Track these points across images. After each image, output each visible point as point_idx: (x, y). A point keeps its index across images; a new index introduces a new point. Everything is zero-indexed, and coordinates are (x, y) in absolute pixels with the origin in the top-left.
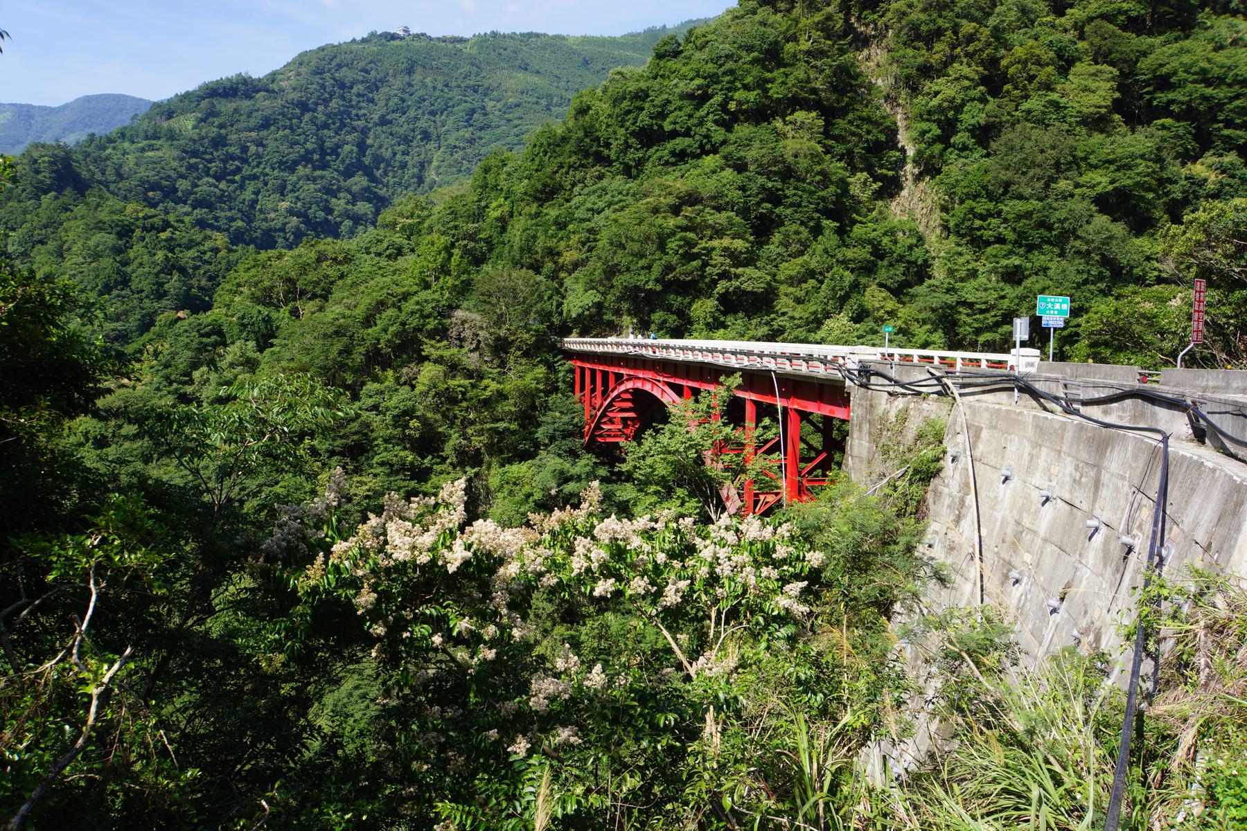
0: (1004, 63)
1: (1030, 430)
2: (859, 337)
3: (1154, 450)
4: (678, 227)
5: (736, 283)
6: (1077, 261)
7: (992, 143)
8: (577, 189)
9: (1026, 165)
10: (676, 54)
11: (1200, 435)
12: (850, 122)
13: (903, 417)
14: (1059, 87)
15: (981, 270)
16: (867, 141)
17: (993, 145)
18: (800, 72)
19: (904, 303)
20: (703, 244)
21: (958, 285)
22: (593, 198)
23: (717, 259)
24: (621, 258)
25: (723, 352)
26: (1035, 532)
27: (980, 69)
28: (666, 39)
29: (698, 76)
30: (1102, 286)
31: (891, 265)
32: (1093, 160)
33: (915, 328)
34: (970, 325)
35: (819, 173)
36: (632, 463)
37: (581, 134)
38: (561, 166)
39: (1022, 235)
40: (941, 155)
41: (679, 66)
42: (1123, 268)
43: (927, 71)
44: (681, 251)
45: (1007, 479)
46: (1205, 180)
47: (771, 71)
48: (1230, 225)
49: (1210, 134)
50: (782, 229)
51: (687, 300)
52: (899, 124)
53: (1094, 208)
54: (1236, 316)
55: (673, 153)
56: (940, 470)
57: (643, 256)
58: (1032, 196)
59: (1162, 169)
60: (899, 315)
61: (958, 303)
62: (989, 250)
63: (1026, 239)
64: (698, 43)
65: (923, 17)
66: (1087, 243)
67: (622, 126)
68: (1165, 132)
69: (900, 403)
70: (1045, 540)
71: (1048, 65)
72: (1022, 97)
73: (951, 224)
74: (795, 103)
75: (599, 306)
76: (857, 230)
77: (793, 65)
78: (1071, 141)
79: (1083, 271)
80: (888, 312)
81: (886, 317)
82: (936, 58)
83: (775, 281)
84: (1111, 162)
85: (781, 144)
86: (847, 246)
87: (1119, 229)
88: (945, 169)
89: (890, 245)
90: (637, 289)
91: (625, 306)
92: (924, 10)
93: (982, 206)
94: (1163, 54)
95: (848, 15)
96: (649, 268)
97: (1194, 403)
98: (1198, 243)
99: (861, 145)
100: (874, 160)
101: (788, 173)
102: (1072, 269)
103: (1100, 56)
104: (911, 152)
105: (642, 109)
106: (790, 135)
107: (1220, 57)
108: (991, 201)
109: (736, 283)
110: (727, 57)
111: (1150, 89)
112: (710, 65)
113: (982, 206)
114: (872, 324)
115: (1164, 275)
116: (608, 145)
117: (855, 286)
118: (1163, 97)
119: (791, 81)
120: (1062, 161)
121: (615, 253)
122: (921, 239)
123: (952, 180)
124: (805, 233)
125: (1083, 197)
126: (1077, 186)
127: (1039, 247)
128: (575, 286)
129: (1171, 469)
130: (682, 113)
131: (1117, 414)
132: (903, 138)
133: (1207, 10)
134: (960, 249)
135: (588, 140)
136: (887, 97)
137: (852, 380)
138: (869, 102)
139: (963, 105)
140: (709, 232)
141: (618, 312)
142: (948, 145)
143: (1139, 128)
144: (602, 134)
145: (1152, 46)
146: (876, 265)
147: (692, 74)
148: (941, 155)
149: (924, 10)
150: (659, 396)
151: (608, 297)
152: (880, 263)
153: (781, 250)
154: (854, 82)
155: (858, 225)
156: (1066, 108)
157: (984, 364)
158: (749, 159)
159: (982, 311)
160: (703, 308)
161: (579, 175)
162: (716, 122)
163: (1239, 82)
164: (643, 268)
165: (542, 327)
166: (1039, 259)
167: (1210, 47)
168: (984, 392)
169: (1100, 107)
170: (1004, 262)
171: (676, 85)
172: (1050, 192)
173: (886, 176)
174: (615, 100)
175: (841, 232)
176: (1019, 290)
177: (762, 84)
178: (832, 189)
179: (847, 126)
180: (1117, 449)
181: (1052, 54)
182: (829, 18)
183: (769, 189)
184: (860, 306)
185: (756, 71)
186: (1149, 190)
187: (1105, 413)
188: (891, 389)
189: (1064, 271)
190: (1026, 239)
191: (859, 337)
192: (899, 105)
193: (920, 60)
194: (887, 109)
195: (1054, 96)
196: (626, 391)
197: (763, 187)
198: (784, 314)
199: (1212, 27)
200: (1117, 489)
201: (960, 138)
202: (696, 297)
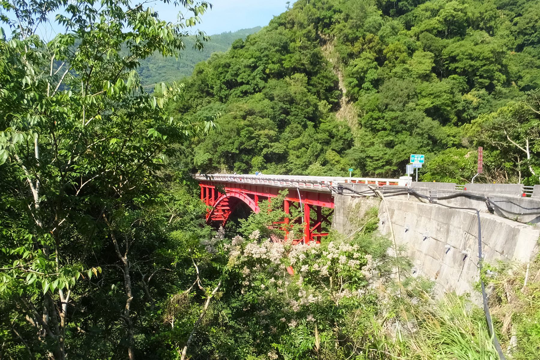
0: (385, 51)
1: (416, 210)
2: (325, 172)
3: (474, 217)
4: (245, 125)
5: (271, 150)
6: (418, 138)
7: (380, 87)
8: (198, 108)
9: (395, 96)
10: (242, 47)
11: (491, 211)
12: (319, 78)
13: (358, 206)
14: (408, 62)
15: (376, 142)
16: (326, 86)
17: (381, 88)
18: (297, 56)
19: (343, 157)
20: (256, 132)
21: (366, 149)
22: (206, 112)
23: (263, 139)
24: (220, 139)
25: (274, 180)
26: (421, 252)
27: (375, 54)
28: (237, 40)
29: (252, 57)
30: (429, 148)
31: (337, 141)
32: (424, 94)
33: (348, 168)
34: (372, 166)
35: (305, 101)
36: (244, 228)
37: (200, 82)
38: (191, 97)
39: (394, 127)
40: (358, 92)
41: (244, 52)
42: (438, 140)
43: (351, 55)
44: (247, 136)
45: (407, 230)
46: (472, 101)
47: (284, 55)
48: (491, 124)
49: (473, 81)
50: (290, 126)
51: (250, 157)
52: (340, 79)
53: (425, 114)
54: (495, 162)
55: (242, 92)
56: (377, 228)
57: (230, 138)
58: (397, 110)
59: (454, 97)
60: (341, 162)
61: (366, 157)
62: (379, 133)
63: (395, 128)
64: (252, 42)
65: (350, 31)
66: (422, 130)
67: (219, 79)
68: (454, 81)
69: (357, 200)
70: (426, 255)
71: (403, 52)
72: (393, 67)
73: (363, 123)
74: (295, 70)
75: (210, 160)
76: (322, 126)
77: (294, 53)
78: (414, 85)
79: (420, 142)
80: (337, 162)
81: (335, 163)
82: (355, 50)
83: (287, 148)
84: (432, 94)
85: (289, 88)
86: (318, 133)
87: (436, 123)
88: (359, 98)
89: (336, 132)
90: (228, 152)
91: (222, 160)
92: (350, 28)
93: (376, 114)
94: (453, 47)
95: (317, 30)
96: (233, 143)
97: (488, 198)
98: (478, 131)
99: (323, 88)
100: (329, 95)
101: (292, 101)
102: (415, 141)
103: (427, 48)
104: (345, 91)
105: (227, 72)
106: (292, 84)
107: (477, 48)
108: (380, 112)
109: (271, 150)
110: (265, 49)
111: (448, 62)
112: (258, 52)
113: (376, 114)
114: (330, 167)
115: (456, 143)
116: (212, 88)
117: (322, 150)
118: (453, 66)
119: (293, 60)
120: (410, 94)
121: (218, 136)
122: (349, 129)
123: (363, 104)
124: (300, 128)
125: (420, 110)
126: (417, 105)
127: (401, 132)
128: (199, 151)
129: (481, 224)
130: (245, 74)
131: (453, 203)
132: (341, 85)
133: (470, 27)
134: (367, 133)
135: (203, 85)
136: (334, 67)
137: (335, 191)
138: (326, 69)
139: (367, 70)
140: (259, 127)
141: (219, 163)
142: (361, 88)
143: (443, 79)
144: (210, 83)
145: (448, 44)
146: (330, 141)
147: (250, 56)
148: (358, 92)
149: (350, 28)
150: (243, 200)
151: (215, 156)
152: (332, 140)
153: (290, 135)
154: (320, 61)
155: (322, 124)
156: (411, 71)
157: (388, 184)
158: (275, 95)
159: (377, 160)
160: (257, 160)
161: (200, 101)
162: (260, 78)
163: (485, 59)
164: (230, 143)
165: (186, 169)
166: (401, 137)
167: (473, 44)
168: (394, 195)
169: (426, 70)
170: (386, 139)
171: (242, 61)
172: (405, 108)
173: (334, 102)
174: (216, 67)
175: (315, 126)
176: (393, 151)
177: (280, 61)
178: (311, 108)
179: (317, 80)
180: (456, 217)
181: (405, 47)
182: (309, 32)
183: (284, 109)
184: (324, 159)
185: (278, 55)
186: (448, 106)
187: (449, 202)
188: (352, 195)
189: (412, 142)
190: (395, 128)
191: (325, 172)
192: (339, 70)
193: (349, 51)
194: (334, 72)
195: (406, 66)
196: (227, 198)
197: (282, 108)
198: (292, 163)
199: (473, 35)
200: (457, 232)
201: (366, 85)
202: (254, 156)
